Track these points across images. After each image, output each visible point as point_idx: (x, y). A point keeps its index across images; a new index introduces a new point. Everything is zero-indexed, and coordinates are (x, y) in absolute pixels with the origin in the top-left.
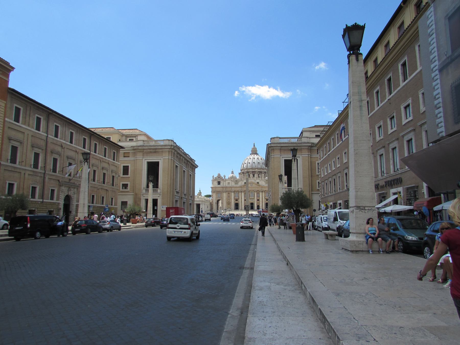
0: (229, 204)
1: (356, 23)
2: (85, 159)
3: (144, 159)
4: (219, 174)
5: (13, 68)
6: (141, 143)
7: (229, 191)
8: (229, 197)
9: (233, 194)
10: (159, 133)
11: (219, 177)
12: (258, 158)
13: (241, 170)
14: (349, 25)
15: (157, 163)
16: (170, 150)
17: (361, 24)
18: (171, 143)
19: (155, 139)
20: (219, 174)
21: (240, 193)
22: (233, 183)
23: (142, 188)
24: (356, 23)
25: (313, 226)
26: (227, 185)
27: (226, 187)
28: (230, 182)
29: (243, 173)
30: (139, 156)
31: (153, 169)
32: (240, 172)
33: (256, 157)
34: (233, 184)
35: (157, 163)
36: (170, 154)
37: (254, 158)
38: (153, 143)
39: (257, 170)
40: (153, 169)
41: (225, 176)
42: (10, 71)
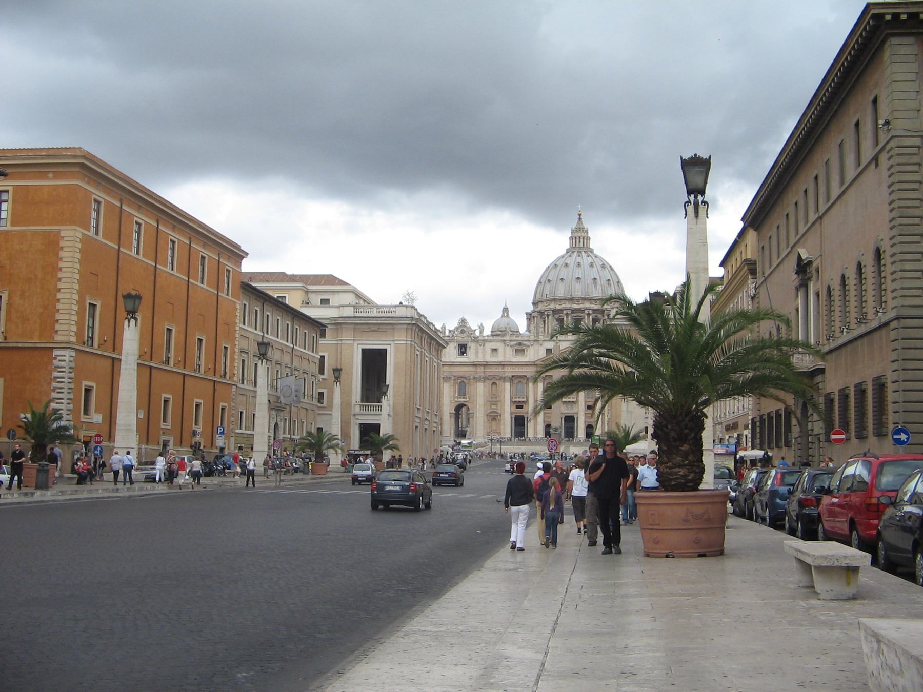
0: (494, 419)
1: (695, 155)
2: (128, 312)
3: (356, 345)
4: (463, 321)
5: (247, 254)
6: (349, 312)
7: (494, 377)
8: (494, 400)
9: (508, 385)
10: (384, 291)
11: (462, 332)
12: (592, 265)
13: (534, 304)
14: (685, 157)
15: (382, 353)
16: (410, 327)
17: (705, 156)
18: (409, 313)
19: (379, 304)
20: (463, 321)
21: (531, 385)
22: (508, 349)
23: (354, 402)
24: (695, 155)
25: (783, 498)
26: (489, 358)
27: (486, 365)
28: (499, 346)
29: (541, 313)
30: (347, 337)
31: (374, 363)
32: (530, 308)
33: (585, 260)
34: (507, 354)
35: (382, 353)
36: (409, 336)
37: (579, 265)
38: (374, 313)
39: (587, 305)
40: (374, 363)
41: (482, 329)
42: (242, 258)
